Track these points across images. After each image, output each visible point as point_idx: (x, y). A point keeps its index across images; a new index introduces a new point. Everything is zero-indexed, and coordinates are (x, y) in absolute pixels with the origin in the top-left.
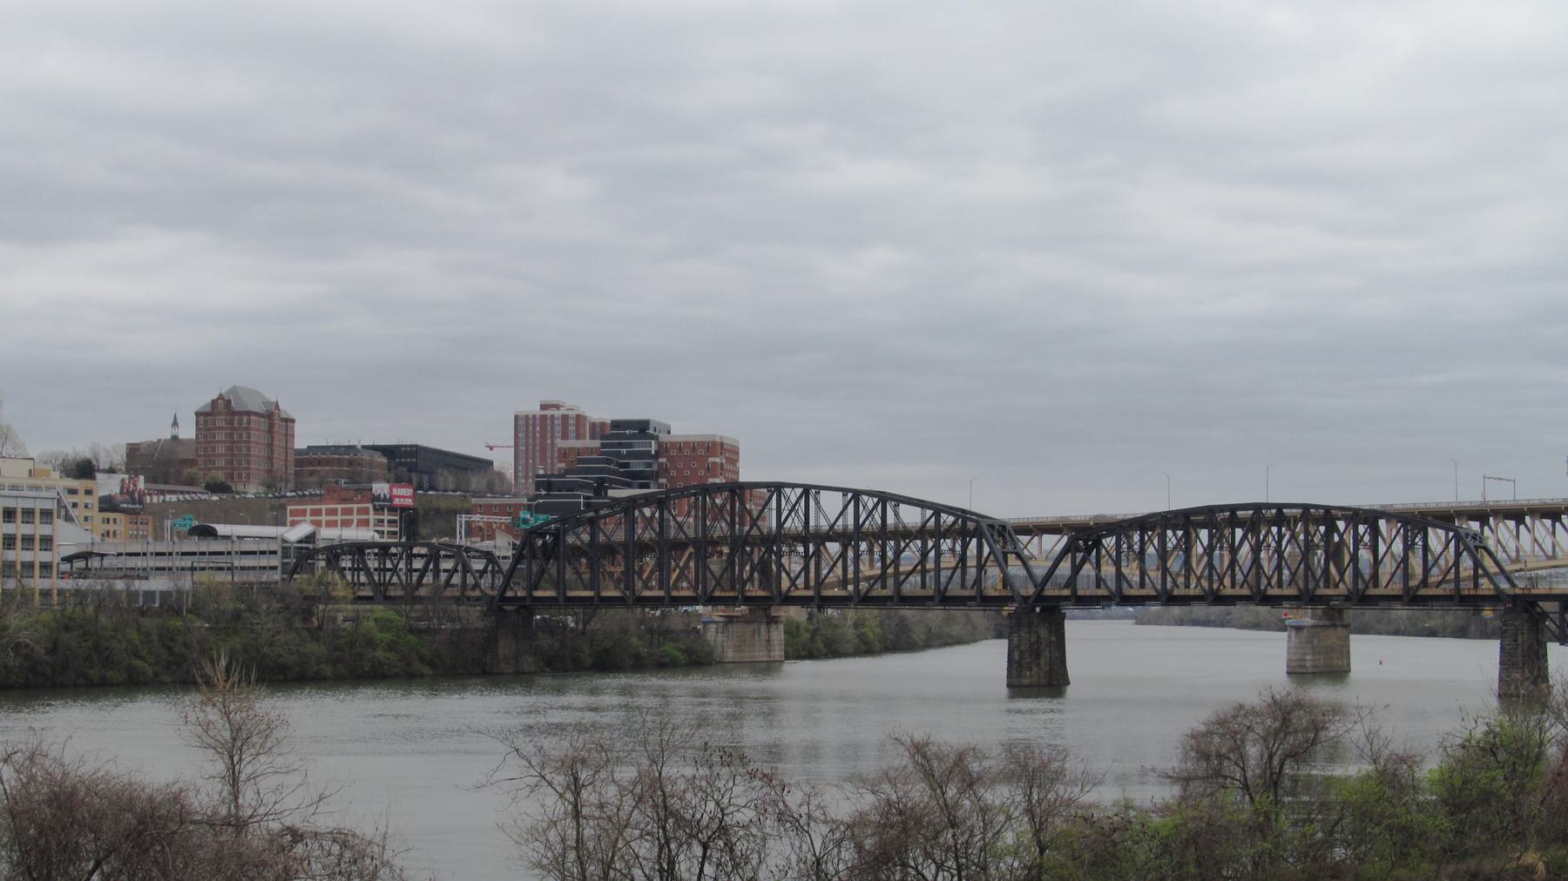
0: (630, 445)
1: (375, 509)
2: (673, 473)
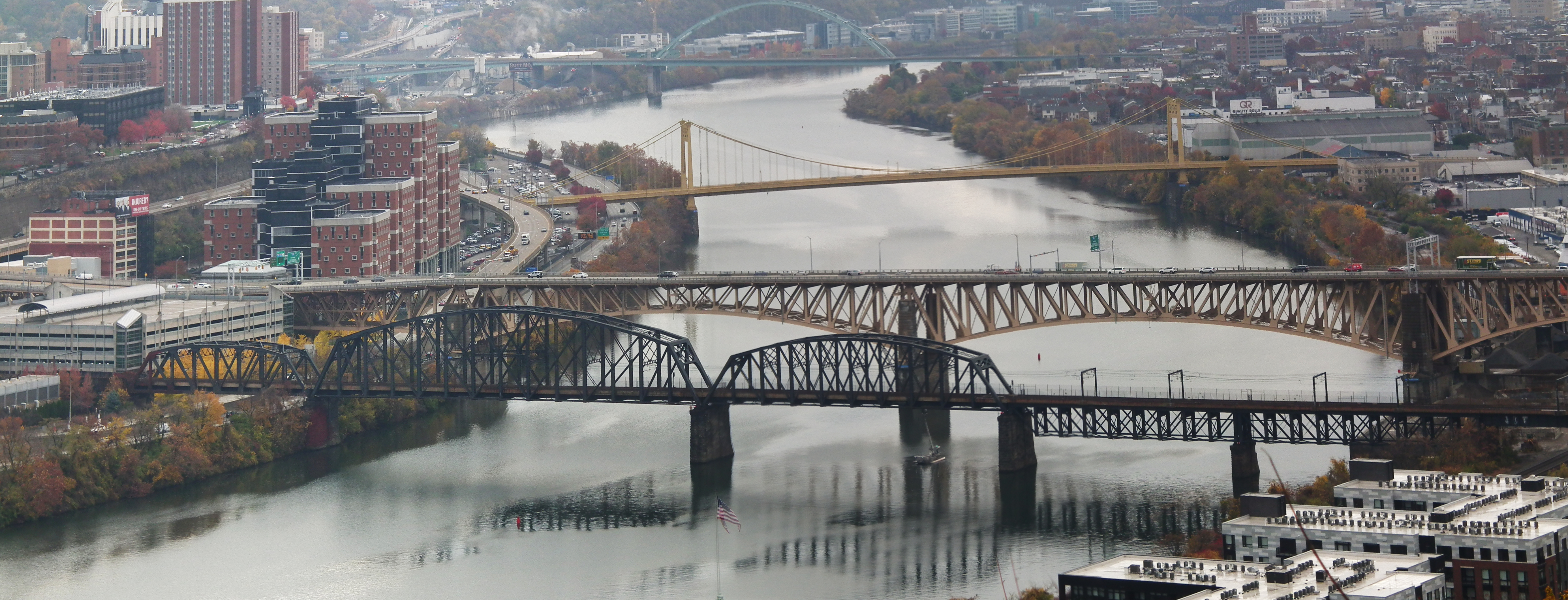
0: (339, 130)
2: (380, 154)
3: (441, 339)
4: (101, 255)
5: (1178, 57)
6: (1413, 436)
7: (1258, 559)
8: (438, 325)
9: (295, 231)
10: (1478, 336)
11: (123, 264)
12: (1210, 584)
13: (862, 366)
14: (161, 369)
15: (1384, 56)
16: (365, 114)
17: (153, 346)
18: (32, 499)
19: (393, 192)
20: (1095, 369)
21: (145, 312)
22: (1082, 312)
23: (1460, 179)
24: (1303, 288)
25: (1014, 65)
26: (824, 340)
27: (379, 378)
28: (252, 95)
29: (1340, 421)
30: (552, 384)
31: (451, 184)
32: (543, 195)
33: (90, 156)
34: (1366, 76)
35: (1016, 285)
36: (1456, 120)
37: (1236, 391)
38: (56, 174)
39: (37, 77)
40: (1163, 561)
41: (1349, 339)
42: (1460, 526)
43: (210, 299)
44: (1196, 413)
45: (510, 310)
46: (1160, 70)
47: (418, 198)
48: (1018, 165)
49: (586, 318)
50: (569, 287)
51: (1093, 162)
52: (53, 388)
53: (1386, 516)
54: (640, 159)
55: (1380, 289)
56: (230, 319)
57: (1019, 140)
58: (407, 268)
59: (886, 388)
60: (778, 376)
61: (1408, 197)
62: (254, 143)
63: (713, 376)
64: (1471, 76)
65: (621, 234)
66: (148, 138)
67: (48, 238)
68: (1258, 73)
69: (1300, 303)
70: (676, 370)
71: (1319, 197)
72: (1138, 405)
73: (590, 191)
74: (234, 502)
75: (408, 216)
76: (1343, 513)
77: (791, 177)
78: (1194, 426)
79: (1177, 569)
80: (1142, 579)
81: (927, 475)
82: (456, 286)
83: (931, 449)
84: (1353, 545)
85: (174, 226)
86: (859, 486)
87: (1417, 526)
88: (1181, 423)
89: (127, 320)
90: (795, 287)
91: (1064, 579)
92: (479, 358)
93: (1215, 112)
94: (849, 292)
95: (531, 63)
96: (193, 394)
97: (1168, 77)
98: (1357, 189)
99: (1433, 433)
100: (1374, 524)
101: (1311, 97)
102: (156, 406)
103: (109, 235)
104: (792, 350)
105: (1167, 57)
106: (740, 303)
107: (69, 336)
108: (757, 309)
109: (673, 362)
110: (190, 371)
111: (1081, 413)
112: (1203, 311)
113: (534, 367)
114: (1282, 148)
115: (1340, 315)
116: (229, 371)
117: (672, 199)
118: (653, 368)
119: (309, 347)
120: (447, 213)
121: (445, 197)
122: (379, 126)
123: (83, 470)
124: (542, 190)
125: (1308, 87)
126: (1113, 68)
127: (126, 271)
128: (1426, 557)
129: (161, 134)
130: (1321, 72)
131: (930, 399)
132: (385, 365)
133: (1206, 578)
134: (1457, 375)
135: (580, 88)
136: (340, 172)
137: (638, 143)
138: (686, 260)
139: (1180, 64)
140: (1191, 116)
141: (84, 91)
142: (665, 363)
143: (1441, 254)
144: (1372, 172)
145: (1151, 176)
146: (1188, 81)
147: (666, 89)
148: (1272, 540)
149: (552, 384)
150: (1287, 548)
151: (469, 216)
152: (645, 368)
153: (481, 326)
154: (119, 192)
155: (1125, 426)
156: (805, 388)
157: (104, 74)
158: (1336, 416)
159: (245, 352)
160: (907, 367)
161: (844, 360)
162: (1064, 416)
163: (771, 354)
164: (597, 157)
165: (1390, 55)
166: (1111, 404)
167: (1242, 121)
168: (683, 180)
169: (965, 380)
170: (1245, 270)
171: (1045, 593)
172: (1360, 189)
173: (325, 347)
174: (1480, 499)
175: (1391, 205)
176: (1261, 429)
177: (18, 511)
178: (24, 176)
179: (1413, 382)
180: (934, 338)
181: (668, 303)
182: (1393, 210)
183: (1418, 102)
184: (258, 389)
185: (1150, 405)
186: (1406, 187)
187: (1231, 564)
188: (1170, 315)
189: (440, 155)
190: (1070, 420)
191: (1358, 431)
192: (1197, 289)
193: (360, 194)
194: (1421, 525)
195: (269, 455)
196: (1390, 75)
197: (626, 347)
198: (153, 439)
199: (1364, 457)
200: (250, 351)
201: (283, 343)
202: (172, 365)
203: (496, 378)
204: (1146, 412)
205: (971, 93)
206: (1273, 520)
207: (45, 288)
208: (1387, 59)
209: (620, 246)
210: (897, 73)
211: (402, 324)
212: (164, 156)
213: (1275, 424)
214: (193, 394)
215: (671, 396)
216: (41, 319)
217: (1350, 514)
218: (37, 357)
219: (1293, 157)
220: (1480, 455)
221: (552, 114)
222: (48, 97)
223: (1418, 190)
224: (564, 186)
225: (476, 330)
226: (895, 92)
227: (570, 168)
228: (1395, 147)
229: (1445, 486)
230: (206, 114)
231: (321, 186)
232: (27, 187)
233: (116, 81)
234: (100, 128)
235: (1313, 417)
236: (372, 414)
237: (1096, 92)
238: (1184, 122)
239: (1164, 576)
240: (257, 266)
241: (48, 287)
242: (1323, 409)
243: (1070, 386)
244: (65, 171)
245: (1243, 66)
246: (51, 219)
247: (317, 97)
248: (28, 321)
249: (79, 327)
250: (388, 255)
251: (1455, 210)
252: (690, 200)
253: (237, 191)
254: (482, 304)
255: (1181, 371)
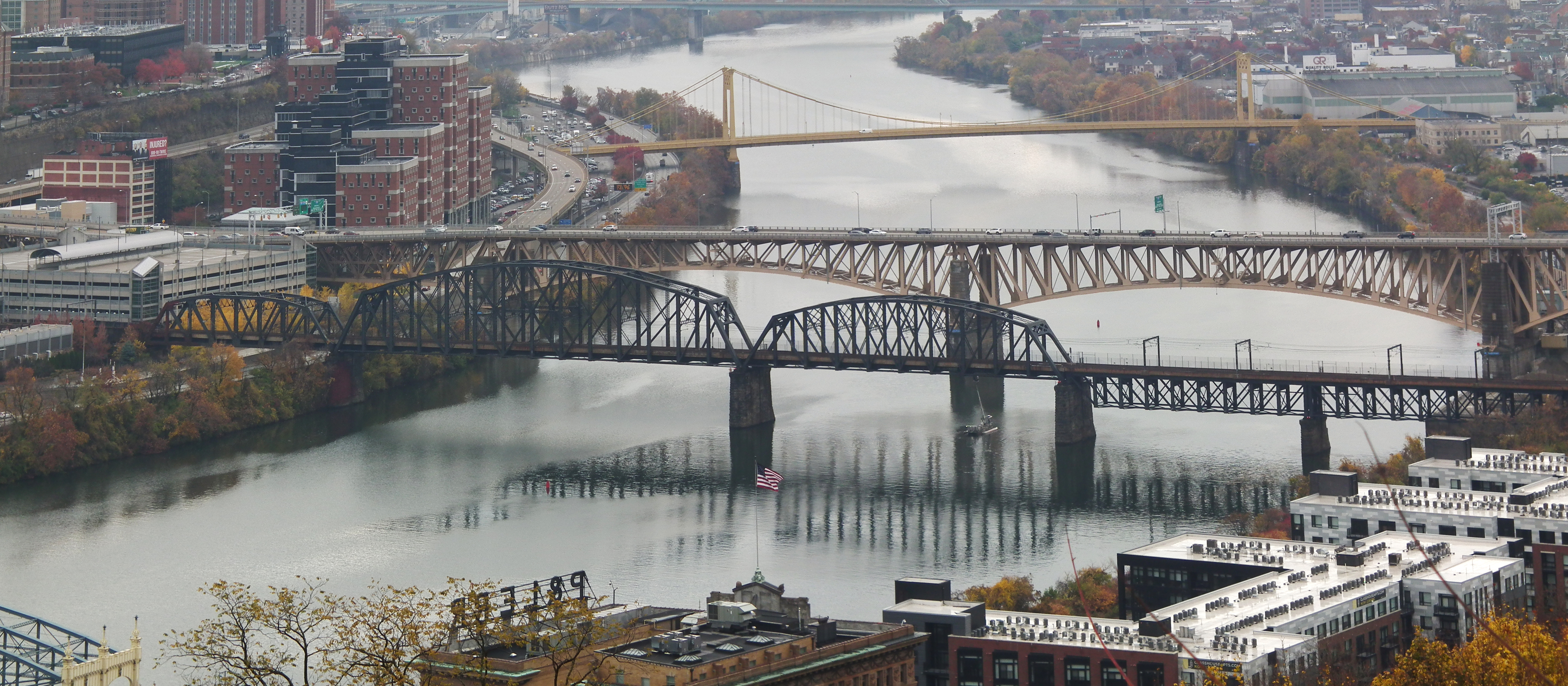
0: (366, 73)
1: (134, 165)
2: (408, 98)
3: (471, 293)
4: (117, 200)
5: (1249, 9)
6: (1492, 413)
7: (1328, 541)
8: (467, 279)
9: (319, 178)
10: (1561, 309)
11: (140, 209)
12: (1277, 566)
13: (911, 330)
14: (178, 319)
15: (1465, 12)
16: (393, 56)
17: (170, 295)
18: (42, 454)
19: (422, 139)
21: (162, 260)
22: (1145, 276)
23: (1544, 143)
24: (1378, 255)
25: (1075, 15)
26: (871, 301)
27: (405, 334)
28: (275, 34)
29: (1415, 396)
30: (585, 342)
31: (482, 130)
32: (578, 144)
33: (106, 96)
34: (1446, 32)
35: (1075, 248)
36: (1540, 80)
37: (1307, 364)
38: (72, 114)
39: (52, 12)
40: (1227, 541)
41: (1426, 310)
42: (1540, 509)
43: (230, 248)
44: (1264, 385)
45: (543, 264)
46: (1229, 23)
47: (447, 145)
48: (1079, 120)
49: (621, 273)
50: (603, 240)
51: (1159, 118)
52: (66, 338)
53: (1463, 496)
54: (679, 107)
55: (1459, 257)
56: (250, 269)
57: (1080, 93)
58: (436, 219)
59: (936, 354)
60: (823, 338)
61: (1489, 160)
62: (278, 85)
63: (754, 337)
64: (1557, 35)
65: (659, 186)
66: (167, 78)
67: (79, 181)
68: (1333, 28)
69: (1375, 271)
70: (716, 330)
71: (1395, 160)
72: (1203, 377)
73: (626, 140)
74: (252, 460)
75: (437, 164)
76: (1418, 493)
77: (838, 129)
78: (1262, 399)
79: (1242, 549)
80: (1205, 560)
81: (979, 447)
82: (486, 238)
83: (983, 419)
84: (1428, 527)
85: (194, 171)
86: (906, 456)
87: (1495, 508)
88: (1248, 396)
89: (144, 268)
90: (842, 245)
91: (1123, 559)
92: (510, 314)
93: (1287, 67)
94: (898, 251)
95: (567, 5)
96: (211, 346)
97: (1237, 30)
98: (1436, 152)
99: (1513, 410)
100: (1451, 505)
101: (1387, 54)
102: (172, 358)
103: (126, 179)
104: (837, 311)
105: (1237, 9)
106: (783, 260)
107: (83, 284)
108: (801, 267)
109: (712, 322)
110: (208, 323)
111: (1143, 384)
112: (1273, 278)
113: (567, 324)
114: (1357, 108)
115: (1417, 284)
116: (249, 323)
117: (713, 149)
118: (691, 327)
119: (332, 300)
120: (478, 161)
121: (475, 145)
122: (408, 69)
123: (97, 424)
124: (576, 138)
125: (1384, 43)
126: (1180, 20)
127: (143, 217)
128: (1504, 541)
129: (181, 74)
130: (1399, 27)
131: (983, 366)
132: (412, 320)
133: (1273, 559)
134: (1539, 349)
135: (618, 33)
136: (367, 116)
137: (678, 91)
138: (726, 216)
139: (1250, 17)
140: (1262, 72)
141: (101, 28)
142: (703, 323)
143: (1524, 222)
144: (1451, 134)
145: (1219, 133)
146: (1258, 35)
147: (708, 34)
148: (1343, 520)
149: (585, 342)
150: (1359, 529)
151: (500, 165)
152: (682, 328)
153: (512, 281)
154: (136, 134)
155: (1189, 398)
156: (851, 352)
157: (122, 10)
158: (1412, 391)
159: (266, 304)
160: (959, 331)
161: (893, 322)
162: (1125, 387)
163: (815, 314)
164: (635, 104)
165: (1472, 12)
166: (1175, 374)
167: (1316, 77)
168: (724, 131)
169: (1021, 347)
170: (1317, 235)
171: (1103, 573)
172: (1439, 152)
173: (350, 300)
174: (1562, 481)
175: (1471, 170)
176: (1333, 403)
177: (28, 465)
178: (38, 116)
179: (1493, 356)
180: (988, 302)
181: (708, 259)
182: (1473, 174)
183: (1500, 61)
184: (279, 343)
185: (1215, 376)
186: (1487, 150)
187: (1299, 544)
188: (1239, 281)
189: (471, 101)
190: (1132, 392)
191: (1434, 407)
192: (1267, 253)
193: (388, 140)
194: (1500, 507)
195: (290, 412)
196: (1471, 32)
197: (663, 305)
198: (169, 393)
199: (1440, 434)
200: (271, 303)
201: (305, 295)
202: (190, 316)
203: (527, 335)
204: (1211, 383)
205: (1030, 43)
206: (1344, 499)
207: (59, 233)
208: (1468, 15)
209: (658, 198)
210: (950, 21)
211: (430, 277)
212: (183, 97)
213: (1347, 399)
214: (211, 346)
215: (711, 357)
216: (54, 266)
217: (1426, 494)
218: (49, 305)
219: (1369, 116)
220: (1562, 434)
221: (588, 58)
222: (63, 34)
223: (1499, 153)
224: (600, 135)
225: (507, 284)
226: (948, 40)
227: (607, 116)
228: (1476, 108)
229: (1525, 467)
230: (227, 54)
231: (346, 130)
232: (41, 127)
233: (134, 18)
234: (117, 66)
235: (1387, 391)
236: (397, 371)
237: (1162, 44)
238: (1254, 77)
239: (1229, 556)
240: (277, 214)
241: (61, 232)
242: (1398, 383)
243: (1132, 356)
244: (80, 111)
245: (1316, 20)
246: (65, 161)
247: (343, 38)
248: (40, 267)
249: (93, 274)
250: (415, 204)
251: (1538, 175)
252: (731, 151)
253: (259, 135)
254: (513, 258)
255: (1249, 341)
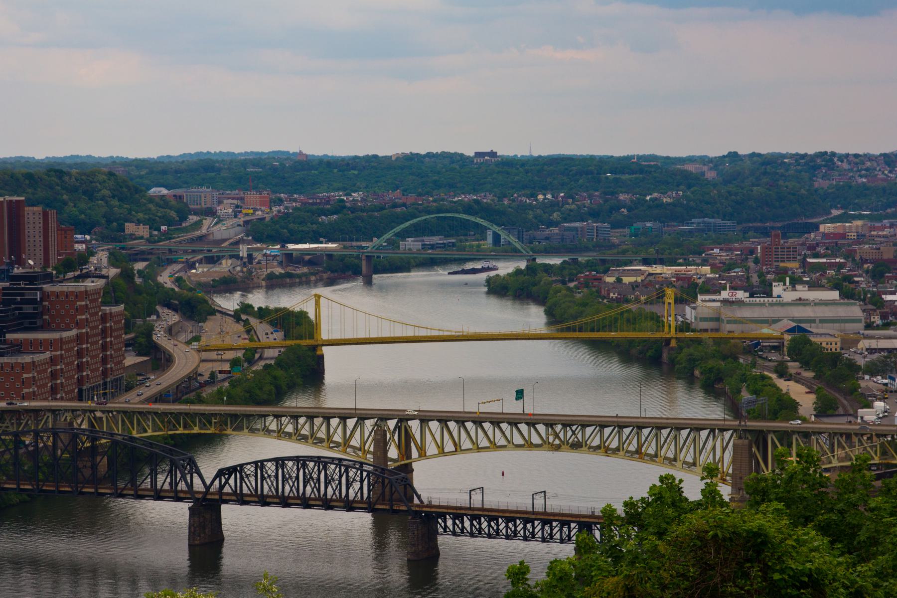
0: (23, 295)
20: (483, 488)
26: (287, 460)
72: (510, 516)
101: (796, 290)
136: (22, 324)
147: (377, 271)
243: (459, 499)
255: (545, 492)
